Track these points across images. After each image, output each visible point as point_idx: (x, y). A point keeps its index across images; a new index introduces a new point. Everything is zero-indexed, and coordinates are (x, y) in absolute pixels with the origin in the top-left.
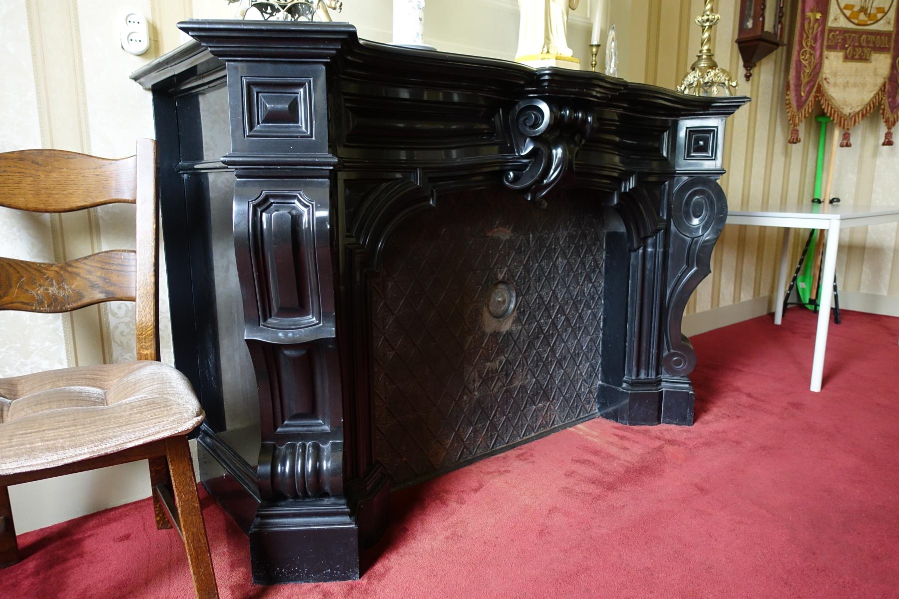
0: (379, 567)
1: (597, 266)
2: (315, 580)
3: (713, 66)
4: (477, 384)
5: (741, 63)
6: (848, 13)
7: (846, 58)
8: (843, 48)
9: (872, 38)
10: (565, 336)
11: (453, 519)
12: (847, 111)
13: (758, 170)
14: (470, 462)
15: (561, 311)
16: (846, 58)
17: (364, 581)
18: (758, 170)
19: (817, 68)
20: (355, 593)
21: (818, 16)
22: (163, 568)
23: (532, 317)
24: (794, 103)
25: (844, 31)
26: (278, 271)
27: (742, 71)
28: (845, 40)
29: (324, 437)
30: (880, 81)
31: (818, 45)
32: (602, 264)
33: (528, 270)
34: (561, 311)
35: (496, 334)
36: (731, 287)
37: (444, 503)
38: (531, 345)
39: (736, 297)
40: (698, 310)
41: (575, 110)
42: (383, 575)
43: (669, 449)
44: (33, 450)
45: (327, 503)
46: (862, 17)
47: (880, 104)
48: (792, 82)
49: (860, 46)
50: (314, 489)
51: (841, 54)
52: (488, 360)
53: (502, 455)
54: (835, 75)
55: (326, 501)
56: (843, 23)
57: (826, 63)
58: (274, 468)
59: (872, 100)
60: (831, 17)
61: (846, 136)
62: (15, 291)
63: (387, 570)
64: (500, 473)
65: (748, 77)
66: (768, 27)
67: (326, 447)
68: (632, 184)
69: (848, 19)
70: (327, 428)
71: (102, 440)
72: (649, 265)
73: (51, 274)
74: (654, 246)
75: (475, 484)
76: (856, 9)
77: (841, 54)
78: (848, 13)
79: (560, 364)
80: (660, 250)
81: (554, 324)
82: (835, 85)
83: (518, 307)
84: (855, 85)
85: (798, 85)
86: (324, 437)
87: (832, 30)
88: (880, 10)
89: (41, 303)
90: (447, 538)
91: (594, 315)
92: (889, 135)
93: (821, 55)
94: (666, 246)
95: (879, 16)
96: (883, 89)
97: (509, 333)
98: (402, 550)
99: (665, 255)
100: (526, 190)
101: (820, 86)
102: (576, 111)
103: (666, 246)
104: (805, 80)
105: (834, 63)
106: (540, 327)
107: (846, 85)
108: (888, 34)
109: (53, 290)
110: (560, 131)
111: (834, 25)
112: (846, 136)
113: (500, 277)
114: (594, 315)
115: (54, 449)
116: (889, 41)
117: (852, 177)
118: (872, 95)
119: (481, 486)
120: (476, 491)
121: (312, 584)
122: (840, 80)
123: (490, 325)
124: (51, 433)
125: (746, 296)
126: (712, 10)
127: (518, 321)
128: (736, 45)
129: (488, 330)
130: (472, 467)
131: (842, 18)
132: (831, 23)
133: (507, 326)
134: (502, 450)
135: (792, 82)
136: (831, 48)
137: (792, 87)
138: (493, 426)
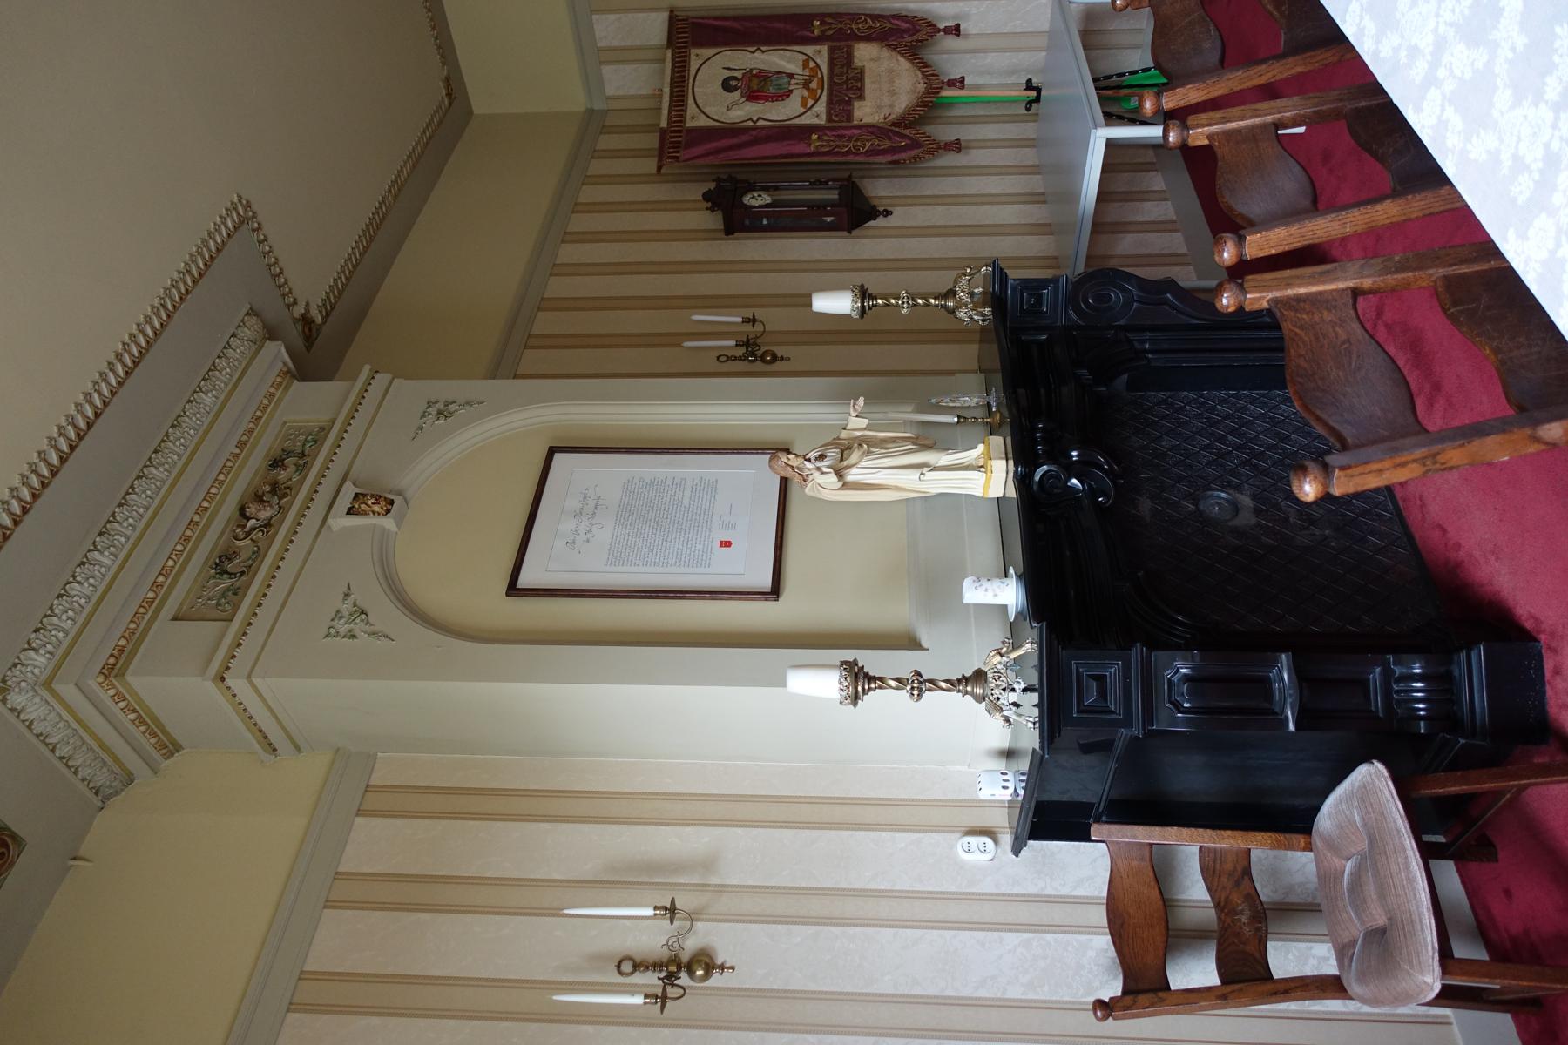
0: (1528, 625)
1: (1165, 401)
2: (1543, 683)
3: (951, 293)
4: (1317, 531)
5: (872, 223)
6: (810, 102)
7: (861, 97)
8: (849, 103)
9: (837, 70)
10: (1251, 434)
11: (1477, 554)
12: (921, 87)
13: (993, 185)
14: (1410, 537)
15: (1222, 439)
16: (861, 97)
17: (1542, 637)
18: (993, 185)
19: (873, 130)
20: (1554, 645)
21: (815, 137)
22: (1537, 837)
23: (1233, 472)
24: (914, 152)
25: (830, 102)
26: (1233, 704)
27: (880, 222)
28: (841, 102)
29: (1387, 674)
30: (886, 53)
31: (847, 132)
32: (1162, 395)
33: (1180, 479)
34: (1222, 439)
35: (1257, 512)
36: (1148, 205)
37: (1459, 564)
38: (1266, 473)
39: (1160, 197)
40: (1184, 250)
41: (1035, 442)
42: (1536, 620)
43: (1388, 315)
44: (1408, 879)
45: (1460, 671)
46: (813, 85)
47: (911, 47)
48: (890, 158)
49: (846, 82)
50: (1442, 684)
51: (856, 104)
52: (1286, 520)
53: (1401, 504)
54: (880, 107)
55: (1456, 673)
56: (821, 107)
57: (867, 120)
58: (1421, 718)
59: (907, 59)
60: (816, 121)
61: (952, 83)
62: (1248, 948)
63: (1532, 616)
64: (1423, 505)
65: (888, 213)
66: (833, 195)
67: (1398, 671)
68: (1085, 372)
69: (817, 101)
70: (1378, 670)
71: (1399, 831)
72: (1165, 346)
73: (1228, 920)
74: (1143, 342)
75: (1437, 533)
76: (806, 94)
77: (856, 104)
78: (810, 102)
79: (1286, 439)
80: (1148, 335)
81: (1238, 447)
82: (891, 106)
83: (1224, 489)
84: (892, 82)
85: (893, 150)
86: (1387, 674)
87: (829, 120)
88: (805, 65)
89: (1258, 929)
90: (1497, 559)
91: (1223, 401)
92: (947, 31)
93: (859, 127)
94: (1142, 329)
95: (812, 64)
96: (894, 48)
97: (1254, 497)
98: (1511, 603)
99: (1153, 329)
100: (1115, 484)
101: (894, 124)
102: (1326, 498)
103: (1142, 329)
104: (888, 144)
105: (866, 112)
106: (1244, 463)
107: (891, 92)
108: (832, 51)
109: (1244, 919)
110: (1056, 455)
111: (824, 116)
112: (952, 83)
113: (1192, 507)
114: (1223, 401)
115: (1407, 864)
116: (839, 48)
117: (990, 58)
118: (902, 60)
119: (1439, 526)
120: (1444, 531)
121: (1548, 688)
122: (886, 100)
123: (1246, 519)
124: (1393, 867)
125: (1157, 182)
126: (897, 298)
127: (1238, 488)
128: (854, 232)
129: (1253, 520)
130: (1417, 536)
131: (816, 109)
132: (822, 121)
133: (1246, 500)
134: (1395, 502)
135: (890, 158)
136: (849, 117)
137: (896, 157)
138: (1365, 513)
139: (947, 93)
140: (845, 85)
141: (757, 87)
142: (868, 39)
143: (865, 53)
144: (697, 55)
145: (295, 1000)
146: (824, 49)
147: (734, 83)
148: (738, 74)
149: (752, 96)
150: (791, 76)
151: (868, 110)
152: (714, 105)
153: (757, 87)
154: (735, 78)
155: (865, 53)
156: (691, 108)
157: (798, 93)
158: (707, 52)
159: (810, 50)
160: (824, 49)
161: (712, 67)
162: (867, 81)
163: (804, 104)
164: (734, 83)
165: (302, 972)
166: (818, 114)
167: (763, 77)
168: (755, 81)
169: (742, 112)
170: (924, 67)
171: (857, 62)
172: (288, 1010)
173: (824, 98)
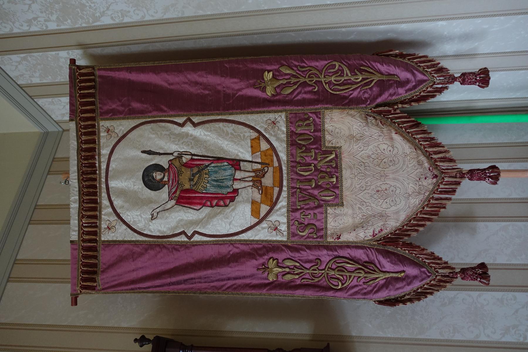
6: (264, 209)
25: (292, 209)
46: (268, 181)
56: (280, 216)
69: (273, 206)
88: (254, 148)
118: (397, 138)
131: (273, 218)
132: (282, 237)
139: (470, 190)
140: (315, 176)
141: (189, 182)
142: (343, 102)
143: (341, 126)
144: (110, 129)
145: (55, 157)
146: (281, 118)
147: (158, 176)
148: (164, 161)
149: (185, 199)
150: (236, 164)
151: (348, 221)
152: (140, 215)
153: (189, 182)
154: (158, 167)
155: (341, 126)
156: (106, 215)
157: (248, 193)
158: (121, 126)
159: (259, 120)
160: (281, 118)
161: (133, 146)
162: (346, 173)
163: (255, 212)
164: (158, 176)
165: (16, 260)
166: (275, 229)
167: (197, 165)
168: (187, 173)
169: (173, 221)
170: (431, 149)
171: (329, 141)
172: (29, 224)
173: (283, 203)
